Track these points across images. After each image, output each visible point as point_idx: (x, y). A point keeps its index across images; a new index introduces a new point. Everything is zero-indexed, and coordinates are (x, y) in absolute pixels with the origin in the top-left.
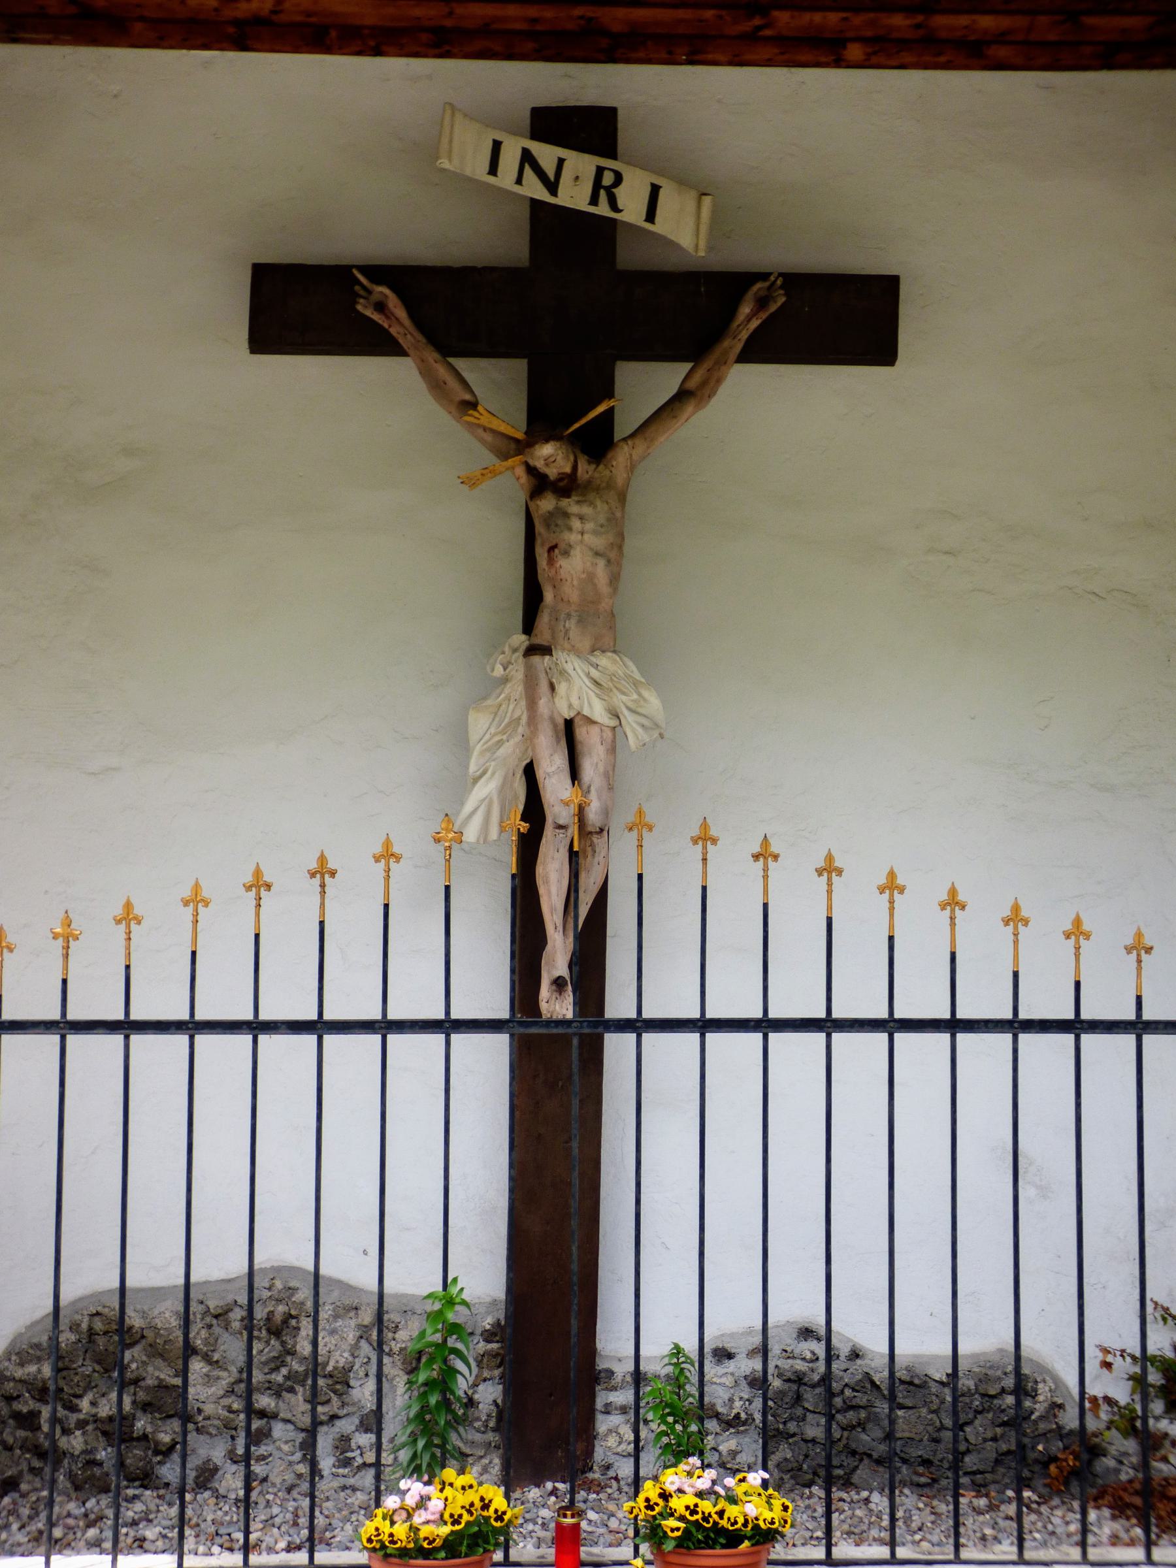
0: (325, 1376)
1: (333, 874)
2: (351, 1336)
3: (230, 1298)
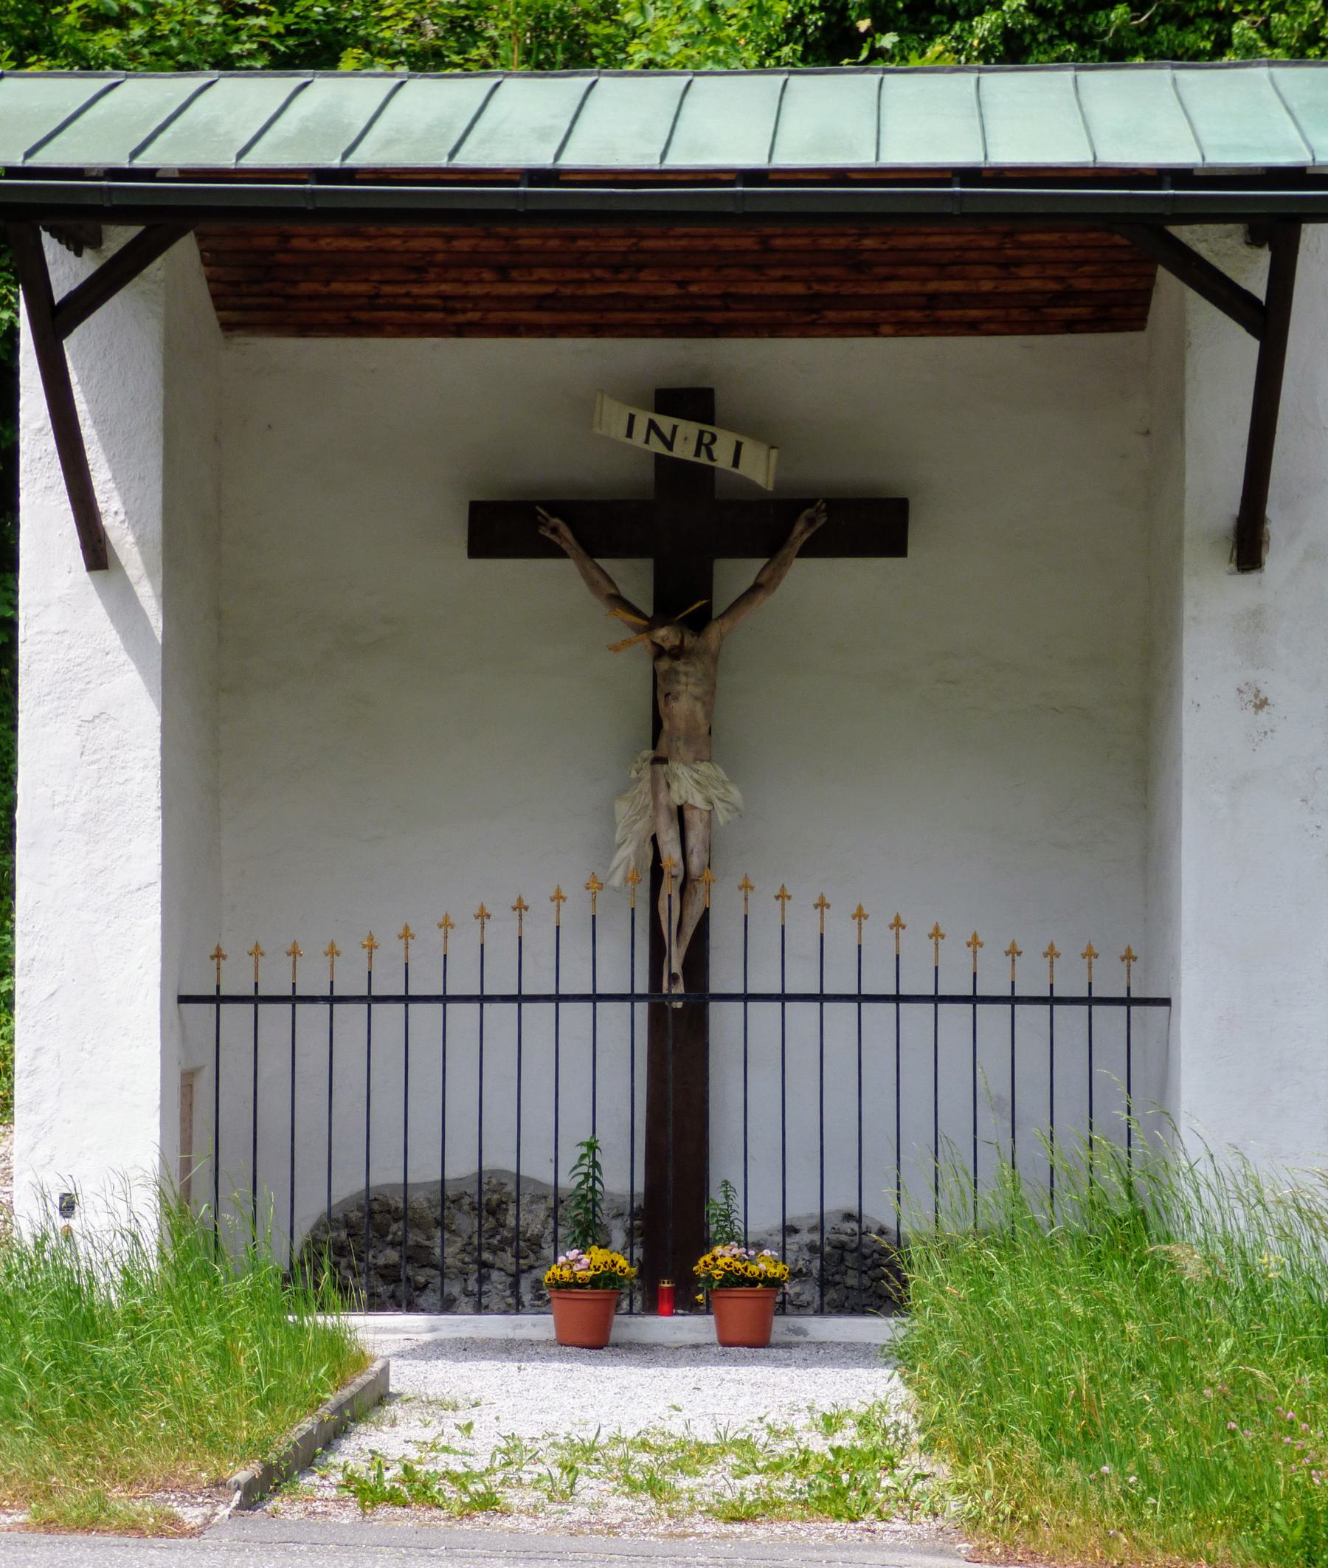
0: (525, 1241)
1: (526, 908)
2: (542, 1215)
3: (462, 1190)
